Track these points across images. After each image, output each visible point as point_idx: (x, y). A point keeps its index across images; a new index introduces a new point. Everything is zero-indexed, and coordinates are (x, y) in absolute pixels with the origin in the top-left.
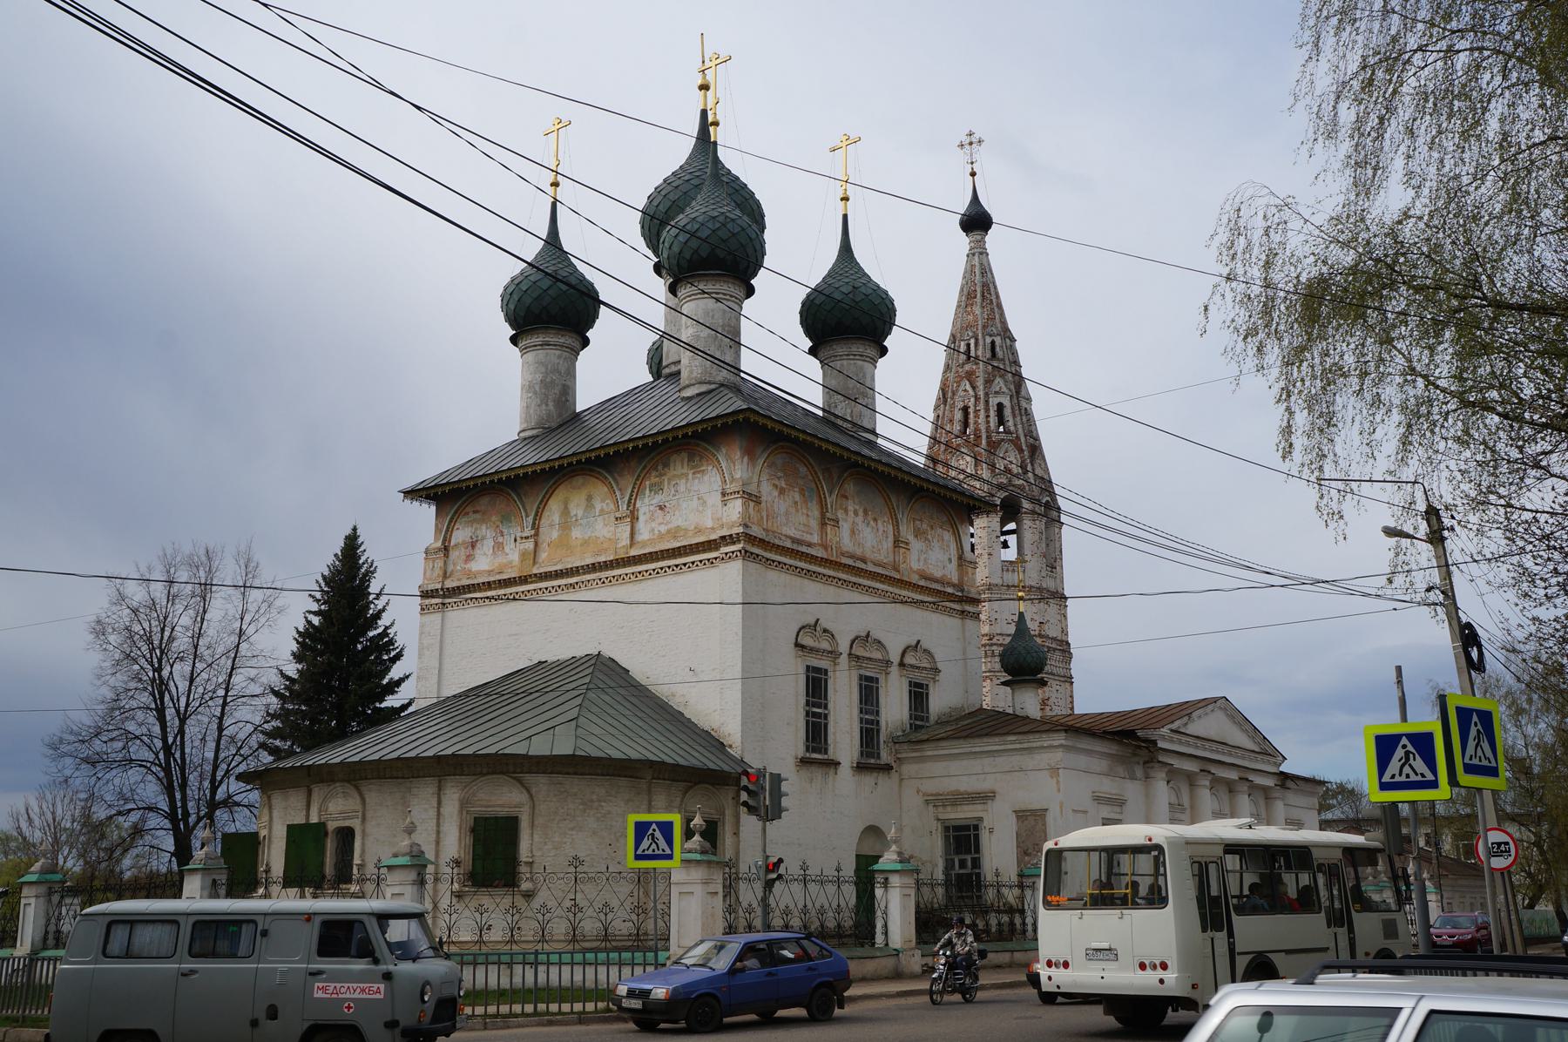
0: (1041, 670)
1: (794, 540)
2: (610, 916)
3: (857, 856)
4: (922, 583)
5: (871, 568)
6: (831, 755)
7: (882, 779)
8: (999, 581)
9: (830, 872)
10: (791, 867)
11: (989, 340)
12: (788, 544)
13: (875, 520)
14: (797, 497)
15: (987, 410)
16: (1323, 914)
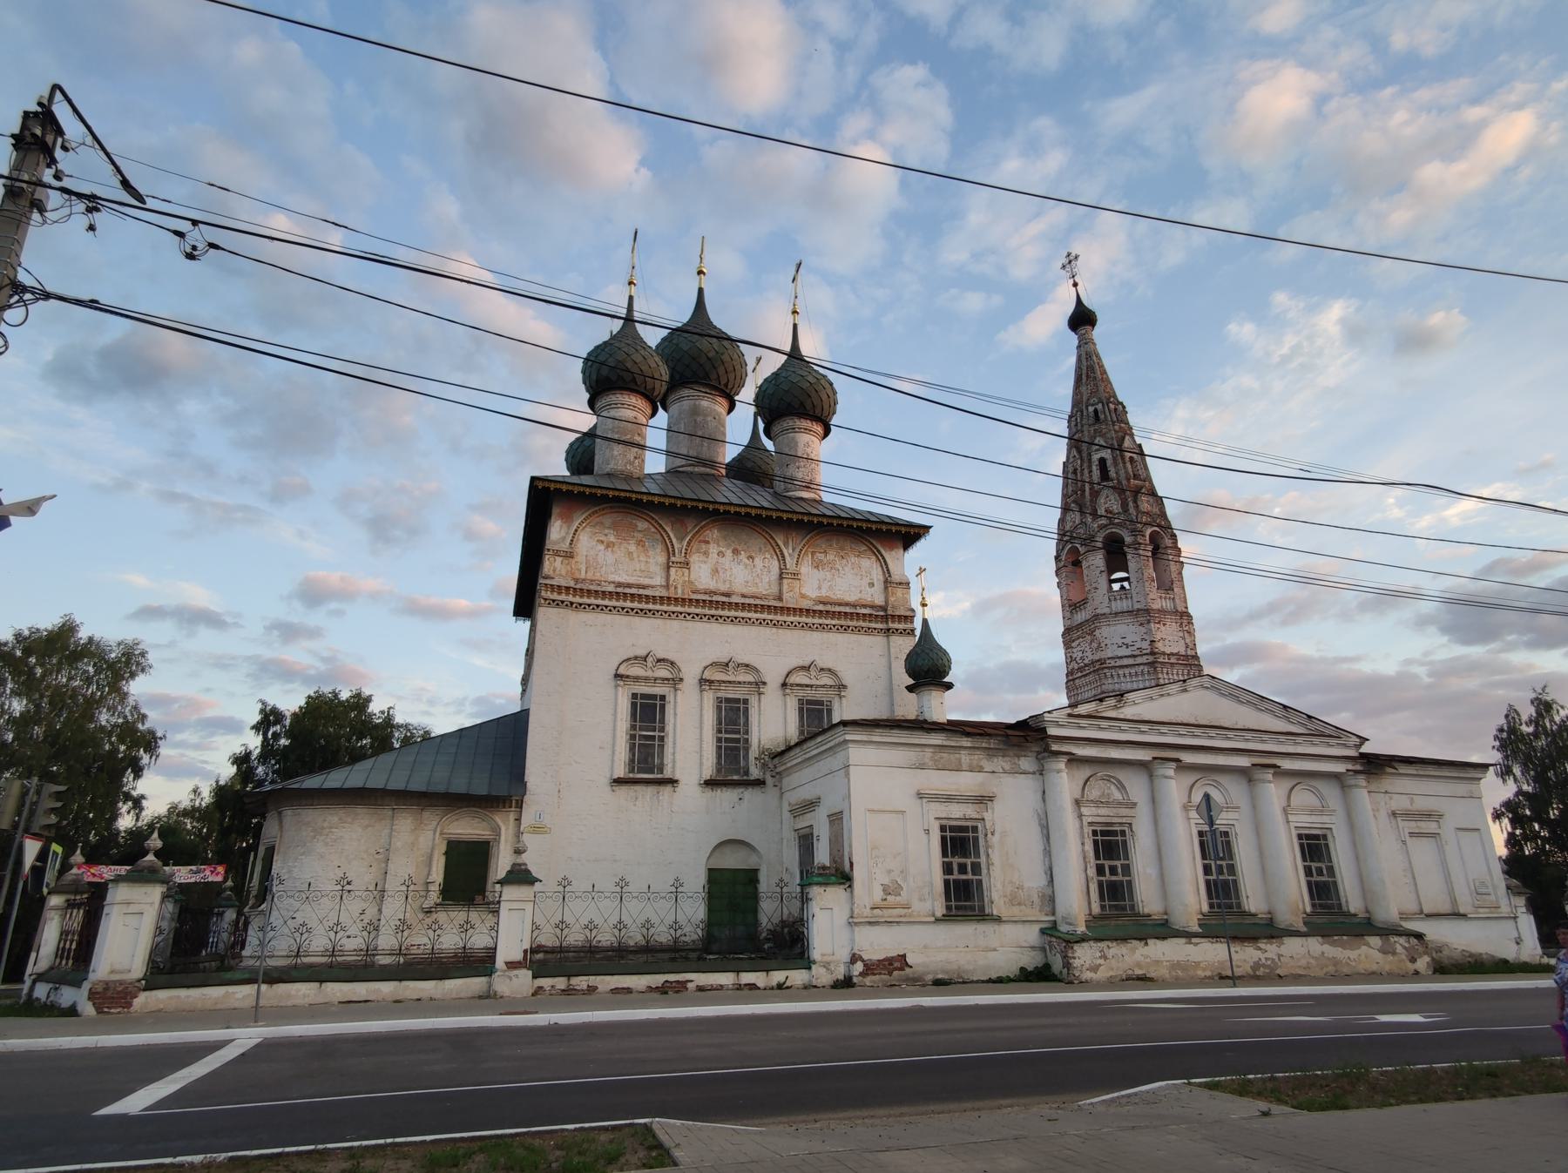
0: (945, 673)
1: (619, 585)
2: (566, 931)
3: (710, 870)
4: (821, 607)
5: (735, 599)
6: (667, 774)
7: (750, 794)
8: (1107, 611)
9: (663, 885)
10: (581, 885)
11: (1091, 409)
12: (611, 588)
13: (751, 557)
14: (632, 548)
15: (1090, 467)
16: (92, 977)
